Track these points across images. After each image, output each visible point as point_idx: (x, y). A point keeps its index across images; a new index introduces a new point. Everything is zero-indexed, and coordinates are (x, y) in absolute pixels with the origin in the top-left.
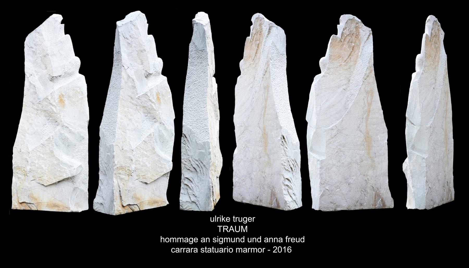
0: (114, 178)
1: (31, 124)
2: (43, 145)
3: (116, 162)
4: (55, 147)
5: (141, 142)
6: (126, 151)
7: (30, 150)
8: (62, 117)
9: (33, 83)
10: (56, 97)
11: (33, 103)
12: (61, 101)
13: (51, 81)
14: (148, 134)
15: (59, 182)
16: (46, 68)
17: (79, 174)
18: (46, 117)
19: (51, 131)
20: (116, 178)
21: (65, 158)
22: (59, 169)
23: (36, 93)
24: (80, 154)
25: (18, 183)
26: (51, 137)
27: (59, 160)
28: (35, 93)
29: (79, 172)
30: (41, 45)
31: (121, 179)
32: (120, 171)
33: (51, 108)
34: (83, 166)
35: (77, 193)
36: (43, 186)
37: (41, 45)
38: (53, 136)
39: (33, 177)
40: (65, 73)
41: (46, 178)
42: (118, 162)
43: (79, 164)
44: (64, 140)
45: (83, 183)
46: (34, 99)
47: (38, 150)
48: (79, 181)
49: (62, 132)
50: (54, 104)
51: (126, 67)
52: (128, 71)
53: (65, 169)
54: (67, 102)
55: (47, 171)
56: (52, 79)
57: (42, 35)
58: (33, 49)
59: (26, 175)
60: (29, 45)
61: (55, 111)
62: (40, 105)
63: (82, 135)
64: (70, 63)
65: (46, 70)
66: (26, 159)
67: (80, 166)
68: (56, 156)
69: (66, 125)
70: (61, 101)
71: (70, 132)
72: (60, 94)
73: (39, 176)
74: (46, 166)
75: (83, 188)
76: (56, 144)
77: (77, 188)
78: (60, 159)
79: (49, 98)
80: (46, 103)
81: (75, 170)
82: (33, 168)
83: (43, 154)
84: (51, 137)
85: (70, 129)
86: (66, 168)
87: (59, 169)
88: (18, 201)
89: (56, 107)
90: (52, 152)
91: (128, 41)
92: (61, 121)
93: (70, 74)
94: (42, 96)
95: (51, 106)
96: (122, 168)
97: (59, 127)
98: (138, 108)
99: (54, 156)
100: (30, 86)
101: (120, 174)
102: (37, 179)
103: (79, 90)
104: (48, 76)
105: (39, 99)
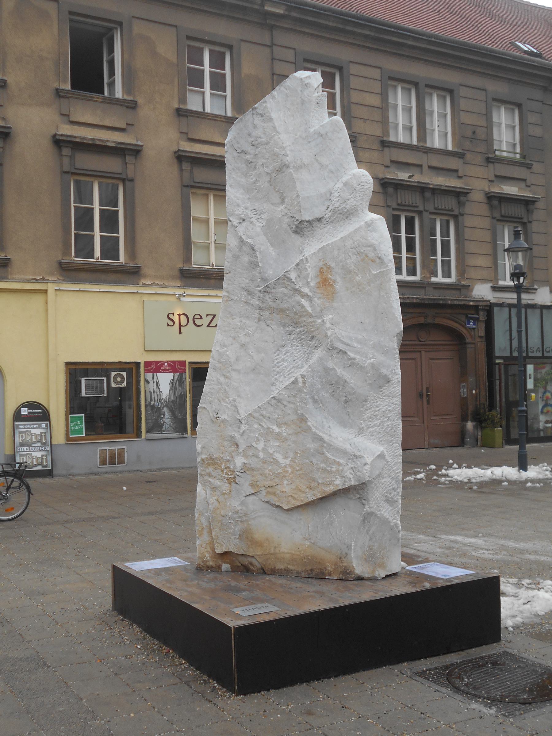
0: (199, 484)
1: (243, 346)
2: (279, 401)
3: (199, 447)
4: (310, 406)
5: (266, 399)
6: (224, 421)
7: (243, 414)
8: (328, 325)
9: (250, 241)
10: (311, 271)
11: (249, 292)
12: (325, 282)
13: (296, 232)
14: (292, 379)
15: (321, 499)
16: (283, 202)
17: (378, 476)
18: (285, 326)
19: (297, 364)
20: (204, 485)
21: (340, 436)
22: (323, 465)
23: (257, 266)
24: (378, 422)
25: (212, 500)
26: (300, 380)
27: (321, 439)
28: (254, 265)
29: (377, 472)
30: (267, 143)
31: (214, 489)
32: (210, 470)
33: (299, 303)
34: (386, 454)
35: (373, 529)
36: (276, 510)
37: (267, 143)
38: (303, 377)
39: (252, 485)
40: (334, 211)
41: (286, 487)
42: (203, 447)
43: (380, 449)
44: (336, 385)
45: (387, 501)
46: (252, 280)
47: (264, 412)
48: (377, 495)
49: (330, 364)
50: (306, 290)
51: (235, 222)
52: (241, 230)
53: (339, 464)
54: (339, 286)
55: (290, 470)
56: (302, 228)
57: (271, 120)
58: (248, 157)
59: (232, 481)
60: (236, 146)
61: (309, 309)
62: (267, 297)
63: (384, 371)
64: (346, 184)
65: (282, 207)
66: (232, 437)
67: (381, 456)
68: (314, 430)
69: (340, 346)
70: (325, 282)
71: (352, 364)
72: (321, 264)
73: (268, 483)
74: (286, 458)
75: (386, 515)
76: (313, 398)
77: (371, 514)
78: (326, 438)
79: (293, 276)
80: (286, 291)
81: (367, 467)
82: (253, 462)
83: (279, 425)
84: (300, 380)
85: (352, 355)
86: (342, 461)
87: (323, 465)
88: (213, 550)
89: (310, 300)
90: (303, 419)
91: (248, 157)
92: (326, 336)
93: (346, 214)
94: (272, 272)
95: (298, 298)
96: (212, 462)
97: (318, 354)
98: (266, 314)
99: (308, 429)
100: (240, 249)
101: (210, 475)
102: (264, 493)
103: (372, 255)
104: (286, 220)
105: (264, 280)
